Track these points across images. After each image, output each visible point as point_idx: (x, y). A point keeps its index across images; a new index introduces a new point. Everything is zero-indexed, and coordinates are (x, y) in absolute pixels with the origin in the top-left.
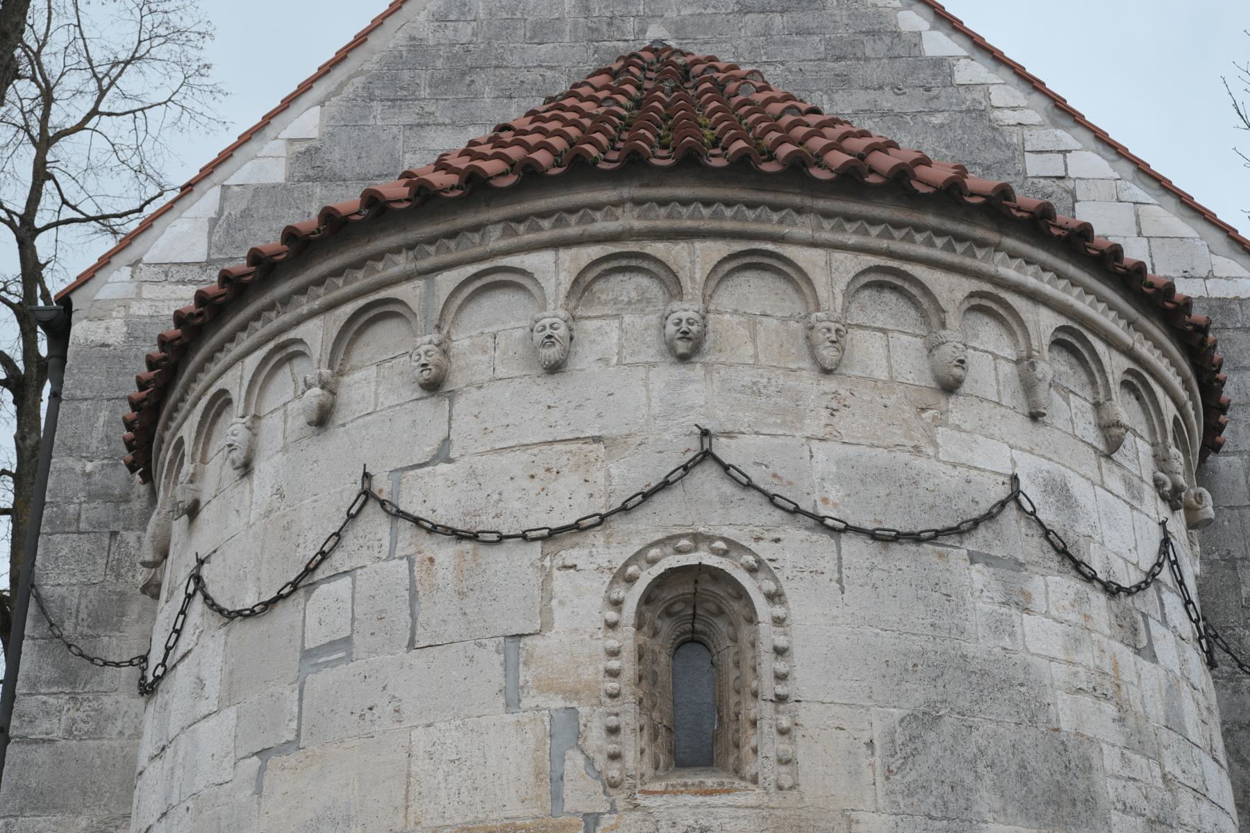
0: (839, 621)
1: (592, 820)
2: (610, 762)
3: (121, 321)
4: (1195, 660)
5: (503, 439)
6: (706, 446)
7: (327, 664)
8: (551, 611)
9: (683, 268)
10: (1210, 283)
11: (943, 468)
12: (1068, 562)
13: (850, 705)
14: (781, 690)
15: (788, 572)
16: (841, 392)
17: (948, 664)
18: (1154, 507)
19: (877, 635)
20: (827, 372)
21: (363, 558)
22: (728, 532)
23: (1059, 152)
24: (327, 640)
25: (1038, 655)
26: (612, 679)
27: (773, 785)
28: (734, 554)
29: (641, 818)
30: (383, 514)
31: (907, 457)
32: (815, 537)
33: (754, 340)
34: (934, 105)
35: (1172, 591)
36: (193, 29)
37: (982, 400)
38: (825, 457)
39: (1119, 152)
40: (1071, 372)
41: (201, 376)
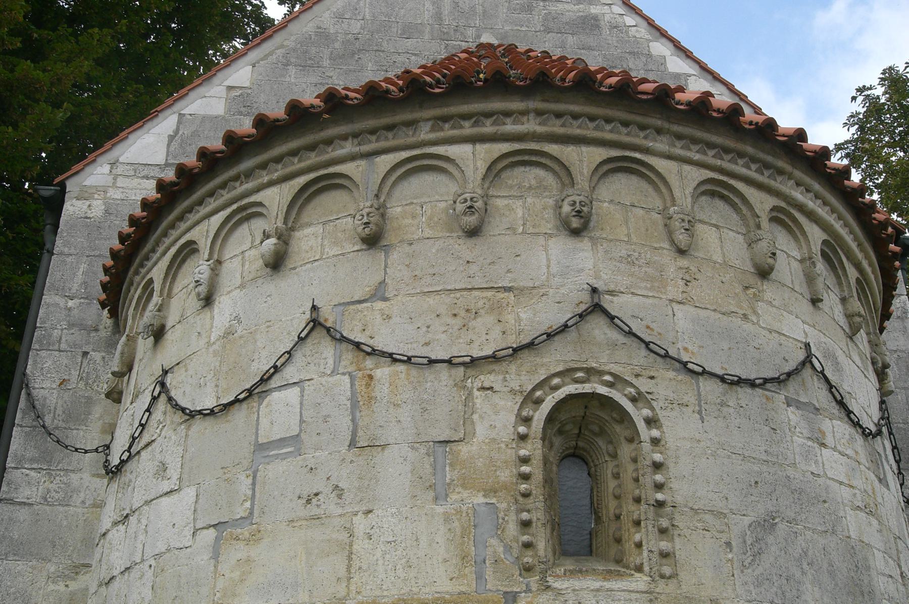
1: (511, 598)
2: (524, 549)
6: (596, 300)
8: (473, 423)
14: (660, 496)
15: (661, 404)
16: (692, 268)
17: (778, 483)
20: (682, 252)
24: (278, 437)
25: (833, 479)
26: (524, 481)
27: (657, 574)
28: (619, 386)
29: (552, 598)
30: (329, 339)
31: (738, 321)
32: (680, 378)
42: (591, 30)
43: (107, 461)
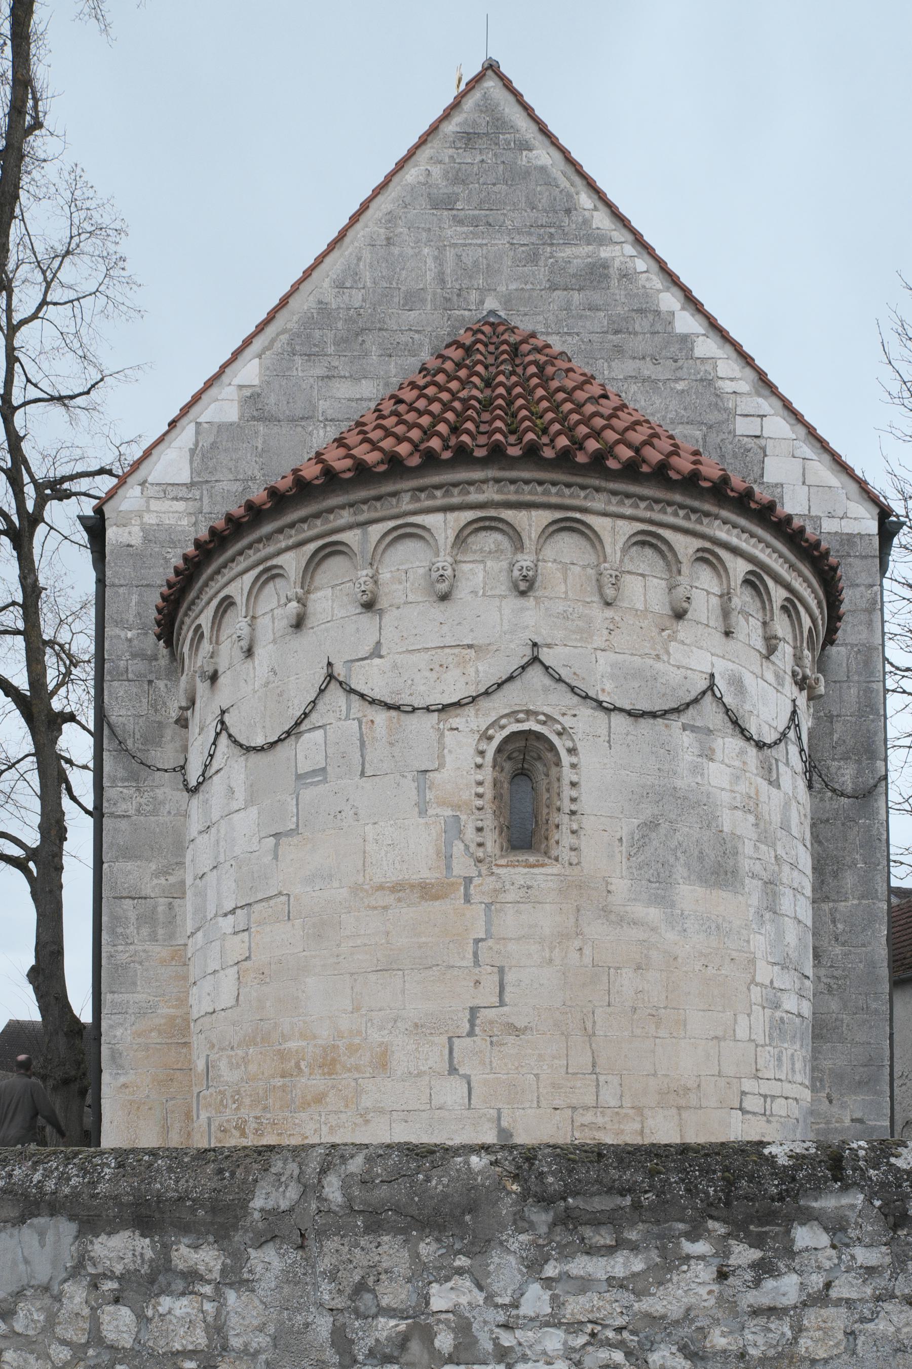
0: (608, 766)
3: (138, 528)
4: (801, 784)
5: (413, 644)
6: (536, 654)
7: (312, 784)
8: (444, 756)
9: (524, 530)
10: (844, 522)
11: (672, 669)
12: (737, 729)
13: (611, 817)
14: (573, 808)
15: (580, 736)
16: (616, 618)
18: (790, 689)
19: (628, 775)
20: (608, 604)
21: (330, 718)
22: (547, 710)
23: (759, 416)
24: (311, 769)
28: (549, 723)
32: (596, 714)
33: (565, 581)
34: (679, 374)
35: (794, 743)
36: (111, 226)
37: (698, 623)
38: (604, 662)
39: (797, 417)
40: (751, 601)
41: (212, 583)
42: (599, 282)
43: (185, 780)
